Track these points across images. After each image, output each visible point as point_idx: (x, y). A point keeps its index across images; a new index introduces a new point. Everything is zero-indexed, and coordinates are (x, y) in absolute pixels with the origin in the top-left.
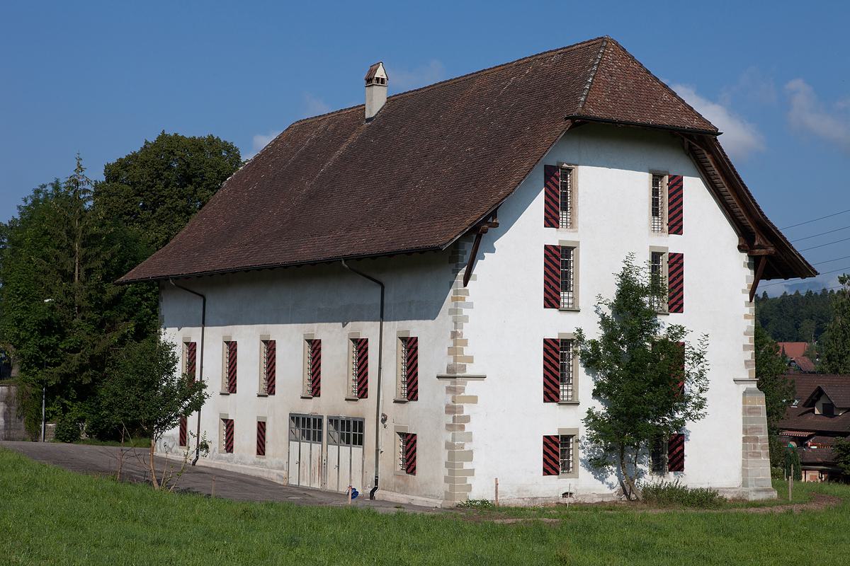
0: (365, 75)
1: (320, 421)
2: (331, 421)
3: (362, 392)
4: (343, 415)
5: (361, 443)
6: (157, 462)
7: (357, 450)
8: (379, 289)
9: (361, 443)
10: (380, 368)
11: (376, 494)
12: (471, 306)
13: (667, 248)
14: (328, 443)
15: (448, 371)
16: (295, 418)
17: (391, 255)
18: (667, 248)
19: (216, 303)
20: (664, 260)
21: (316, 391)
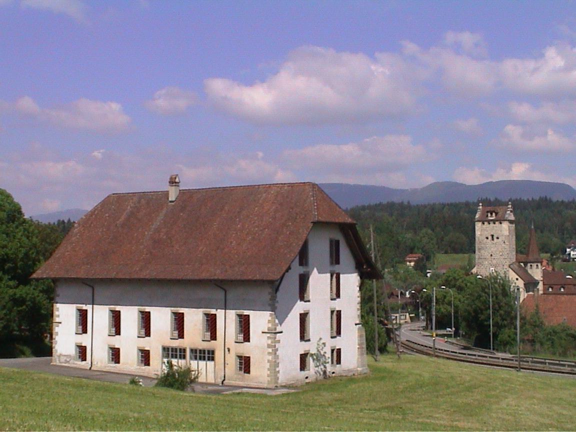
0: (230, 351)
1: (185, 350)
2: (192, 350)
3: (214, 337)
4: (201, 348)
5: (213, 359)
6: (433, 355)
7: (210, 364)
8: (224, 292)
9: (213, 359)
10: (225, 318)
11: (224, 382)
12: (278, 302)
13: (335, 308)
14: (191, 359)
15: (268, 330)
16: (165, 349)
17: (232, 281)
18: (335, 308)
19: (100, 291)
20: (335, 313)
21: (181, 335)
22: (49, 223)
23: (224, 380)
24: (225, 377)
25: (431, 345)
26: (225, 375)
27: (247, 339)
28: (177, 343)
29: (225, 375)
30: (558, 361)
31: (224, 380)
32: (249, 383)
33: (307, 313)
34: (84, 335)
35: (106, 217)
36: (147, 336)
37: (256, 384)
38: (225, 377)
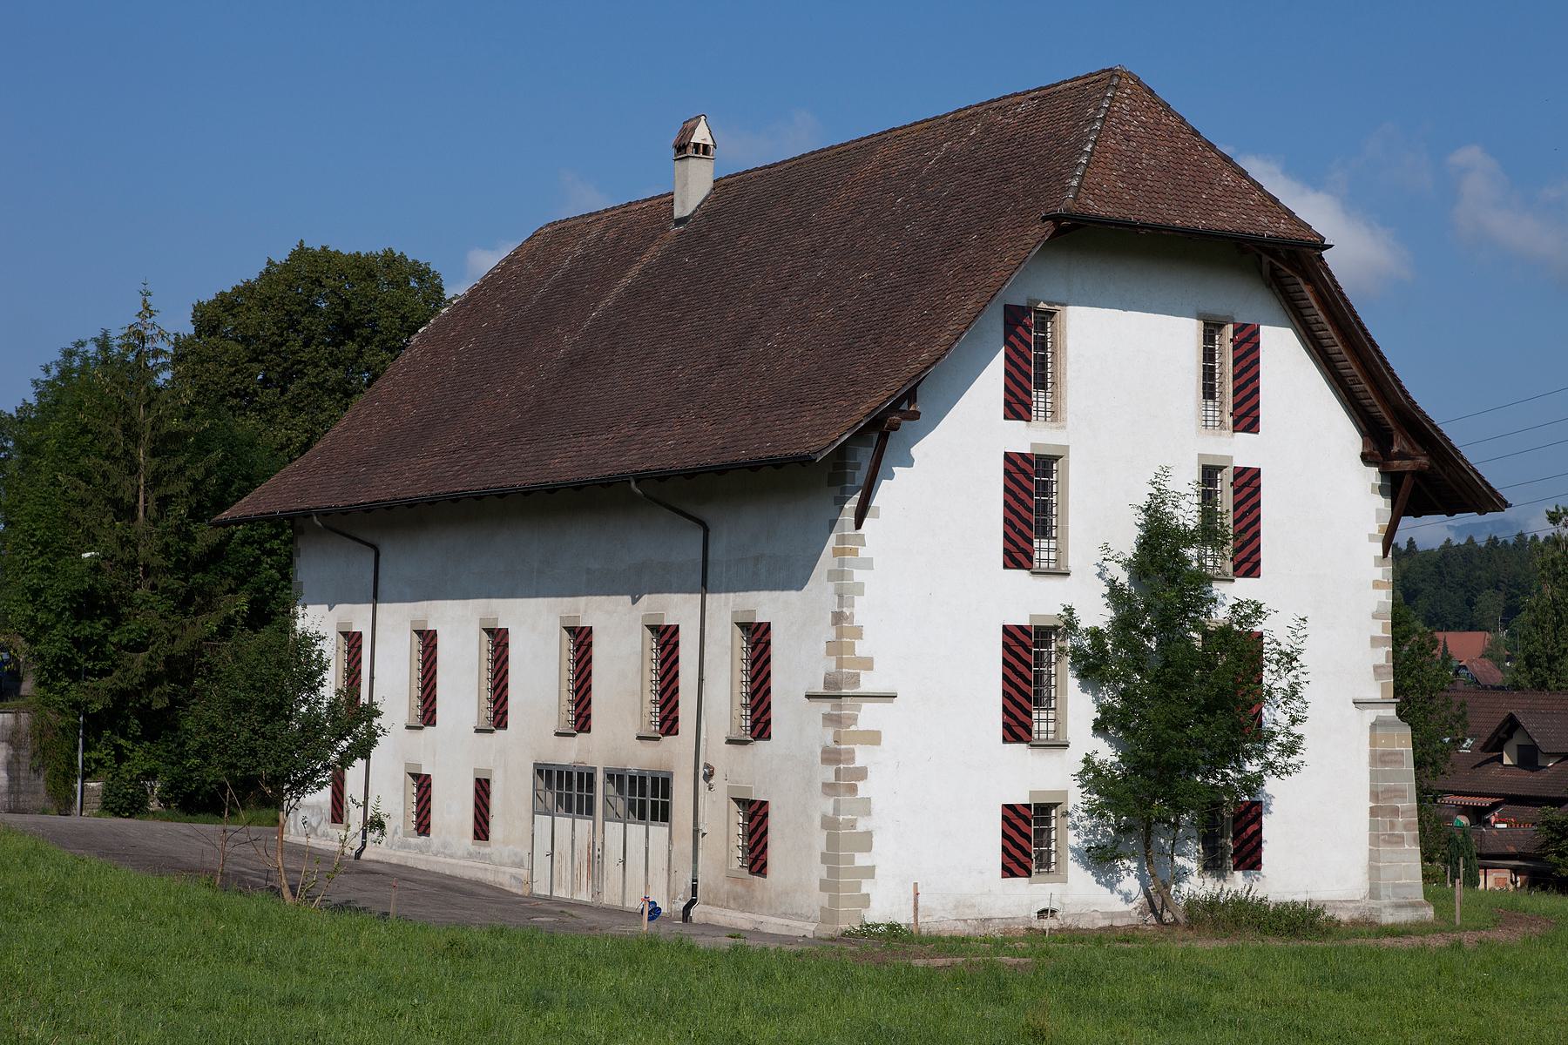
1: (591, 777)
2: (610, 777)
3: (669, 724)
5: (662, 814)
7: (658, 831)
11: (694, 911)
16: (545, 773)
19: (399, 560)
21: (582, 722)
22: (358, 253)
23: (692, 903)
24: (694, 888)
25: (759, 814)
26: (695, 880)
27: (760, 727)
28: (570, 753)
29: (695, 880)
30: (1056, 694)
31: (692, 903)
32: (763, 918)
33: (1056, 458)
34: (498, 732)
35: (902, 206)
36: (580, 730)
37: (1403, 901)
38: (694, 888)
